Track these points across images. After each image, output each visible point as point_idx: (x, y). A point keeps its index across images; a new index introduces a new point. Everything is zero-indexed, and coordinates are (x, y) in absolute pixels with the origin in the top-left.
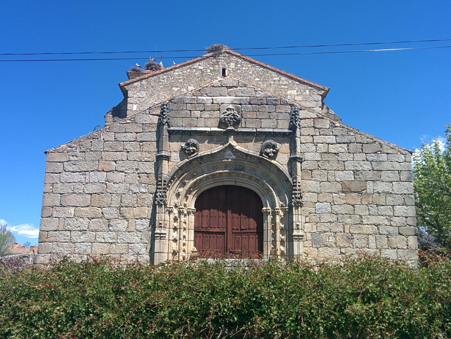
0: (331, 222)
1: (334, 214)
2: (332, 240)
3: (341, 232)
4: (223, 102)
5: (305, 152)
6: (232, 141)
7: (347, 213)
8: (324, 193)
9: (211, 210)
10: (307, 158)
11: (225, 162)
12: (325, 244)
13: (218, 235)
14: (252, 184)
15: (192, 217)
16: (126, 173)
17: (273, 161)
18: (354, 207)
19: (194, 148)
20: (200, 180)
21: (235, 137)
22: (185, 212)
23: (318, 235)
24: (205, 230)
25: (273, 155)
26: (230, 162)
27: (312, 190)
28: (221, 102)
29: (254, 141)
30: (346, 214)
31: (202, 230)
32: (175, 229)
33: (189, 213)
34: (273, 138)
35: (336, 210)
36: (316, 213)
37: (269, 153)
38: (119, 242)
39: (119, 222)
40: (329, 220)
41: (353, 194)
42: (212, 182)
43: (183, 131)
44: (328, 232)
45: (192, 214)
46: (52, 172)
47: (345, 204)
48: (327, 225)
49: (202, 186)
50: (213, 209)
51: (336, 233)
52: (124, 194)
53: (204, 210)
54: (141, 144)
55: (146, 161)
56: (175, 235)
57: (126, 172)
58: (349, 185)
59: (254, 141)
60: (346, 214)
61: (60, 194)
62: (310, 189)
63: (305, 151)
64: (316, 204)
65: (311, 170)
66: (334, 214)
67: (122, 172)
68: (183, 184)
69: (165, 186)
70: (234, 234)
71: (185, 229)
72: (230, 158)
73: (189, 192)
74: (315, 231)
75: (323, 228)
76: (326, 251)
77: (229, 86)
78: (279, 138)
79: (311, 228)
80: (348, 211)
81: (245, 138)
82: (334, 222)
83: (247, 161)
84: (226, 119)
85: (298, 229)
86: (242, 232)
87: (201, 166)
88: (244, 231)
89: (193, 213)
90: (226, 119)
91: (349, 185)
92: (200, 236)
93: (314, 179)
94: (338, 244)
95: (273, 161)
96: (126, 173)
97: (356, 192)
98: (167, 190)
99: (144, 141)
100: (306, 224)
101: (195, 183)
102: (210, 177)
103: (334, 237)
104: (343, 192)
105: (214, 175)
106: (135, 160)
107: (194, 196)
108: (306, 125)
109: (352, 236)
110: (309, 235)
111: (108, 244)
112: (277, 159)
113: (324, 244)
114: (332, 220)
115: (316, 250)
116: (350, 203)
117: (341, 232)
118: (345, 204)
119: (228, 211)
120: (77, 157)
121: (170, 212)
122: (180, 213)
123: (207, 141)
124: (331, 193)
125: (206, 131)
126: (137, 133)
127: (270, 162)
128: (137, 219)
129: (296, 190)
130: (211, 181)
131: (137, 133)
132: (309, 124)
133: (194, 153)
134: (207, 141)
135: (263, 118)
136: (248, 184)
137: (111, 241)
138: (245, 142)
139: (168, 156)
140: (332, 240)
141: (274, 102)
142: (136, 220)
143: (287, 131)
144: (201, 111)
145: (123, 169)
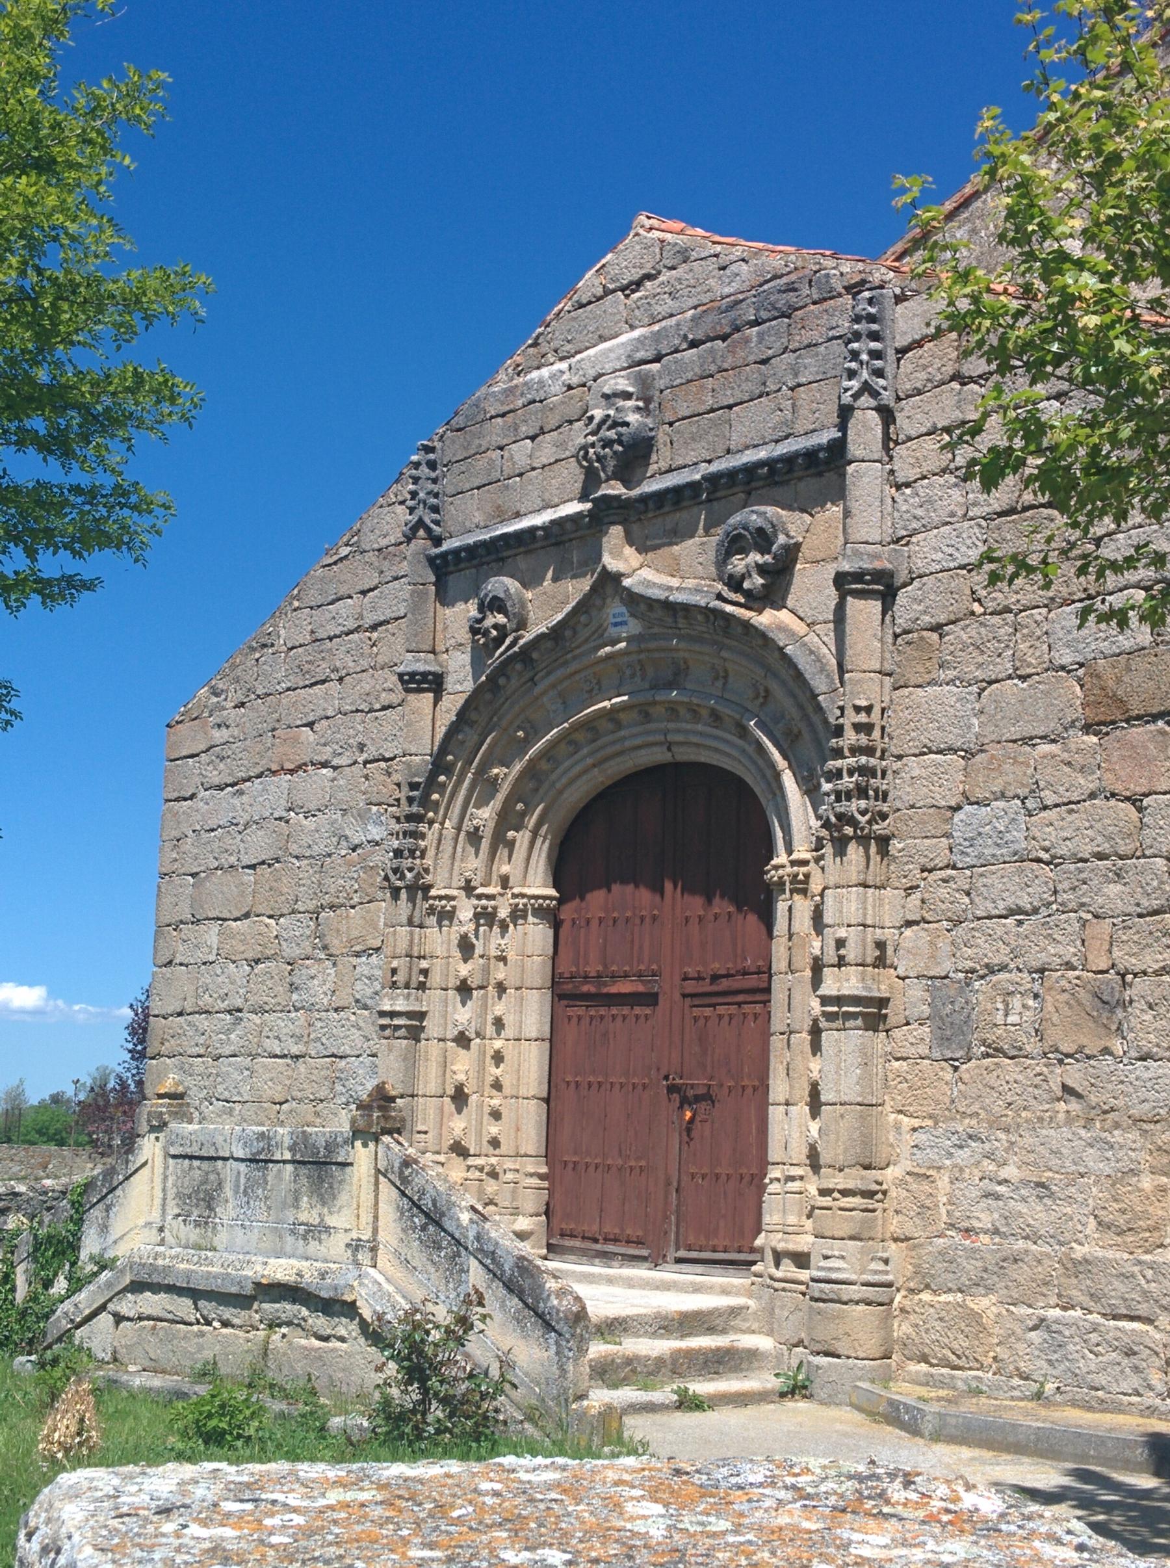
0: (1019, 911)
1: (1039, 860)
2: (1020, 1013)
3: (1069, 966)
4: (598, 369)
5: (915, 532)
6: (619, 556)
7: (1106, 848)
8: (994, 750)
9: (616, 888)
10: (919, 565)
11: (609, 657)
12: (991, 1038)
13: (638, 1010)
14: (722, 746)
15: (535, 936)
16: (335, 768)
17: (765, 619)
18: (1140, 810)
19: (501, 619)
20: (547, 754)
21: (635, 527)
22: (503, 913)
23: (961, 991)
24: (593, 990)
25: (761, 581)
26: (621, 653)
27: (941, 742)
28: (592, 373)
29: (701, 531)
30: (1101, 856)
31: (585, 988)
32: (464, 989)
33: (517, 915)
34: (778, 492)
35: (1050, 835)
36: (954, 867)
37: (743, 578)
38: (313, 1053)
39: (313, 972)
40: (1011, 902)
41: (1138, 733)
42: (589, 761)
43: (770, 463)
44: (1003, 968)
45: (531, 919)
46: (176, 795)
47: (1093, 796)
48: (1000, 931)
49: (558, 785)
50: (624, 882)
51: (1041, 971)
52: (330, 855)
53: (592, 890)
54: (375, 635)
55: (384, 708)
56: (464, 1015)
57: (335, 762)
58: (1119, 680)
59: (701, 531)
60: (1101, 856)
61: (193, 875)
62: (932, 735)
63: (915, 525)
64: (959, 816)
65: (937, 628)
66: (1039, 860)
67: (324, 765)
68: (486, 788)
69: (415, 809)
70: (688, 1000)
71: (501, 988)
72: (620, 637)
73: (508, 820)
74: (946, 966)
75: (987, 950)
76: (991, 1079)
77: (631, 283)
78: (802, 486)
79: (926, 950)
80: (1109, 838)
81: (670, 520)
82: (1036, 911)
83: (681, 638)
84: (591, 451)
85: (841, 962)
86: (714, 988)
87: (537, 690)
88: (725, 984)
89: (539, 912)
90: (591, 451)
91: (1119, 680)
92: (579, 1018)
93: (951, 674)
94: (1054, 1035)
95: (765, 619)
96: (335, 768)
97: (1155, 717)
98: (431, 823)
99: (381, 624)
100: (908, 932)
101: (530, 772)
102: (579, 737)
103: (1036, 996)
104: (1087, 728)
105: (588, 725)
106: (357, 711)
107: (535, 833)
108: (923, 375)
109: (1124, 984)
110: (916, 992)
111: (289, 1061)
112: (790, 602)
113: (984, 1042)
114: (1025, 902)
115: (948, 1075)
116: (1118, 788)
117: (1069, 966)
118: (1093, 796)
119: (668, 886)
120: (228, 727)
121: (447, 916)
122: (486, 917)
123: (550, 574)
124: (1027, 740)
125: (533, 530)
126: (364, 593)
127: (746, 625)
128: (358, 955)
129: (838, 753)
130: (585, 757)
131: (364, 593)
132: (938, 363)
133: (499, 641)
134: (550, 574)
135: (740, 396)
136: (716, 750)
137: (295, 1050)
138: (671, 544)
139: (433, 674)
140: (1020, 1013)
141: (782, 301)
142: (355, 961)
143: (574, 508)
144: (533, 438)
145: (326, 754)
